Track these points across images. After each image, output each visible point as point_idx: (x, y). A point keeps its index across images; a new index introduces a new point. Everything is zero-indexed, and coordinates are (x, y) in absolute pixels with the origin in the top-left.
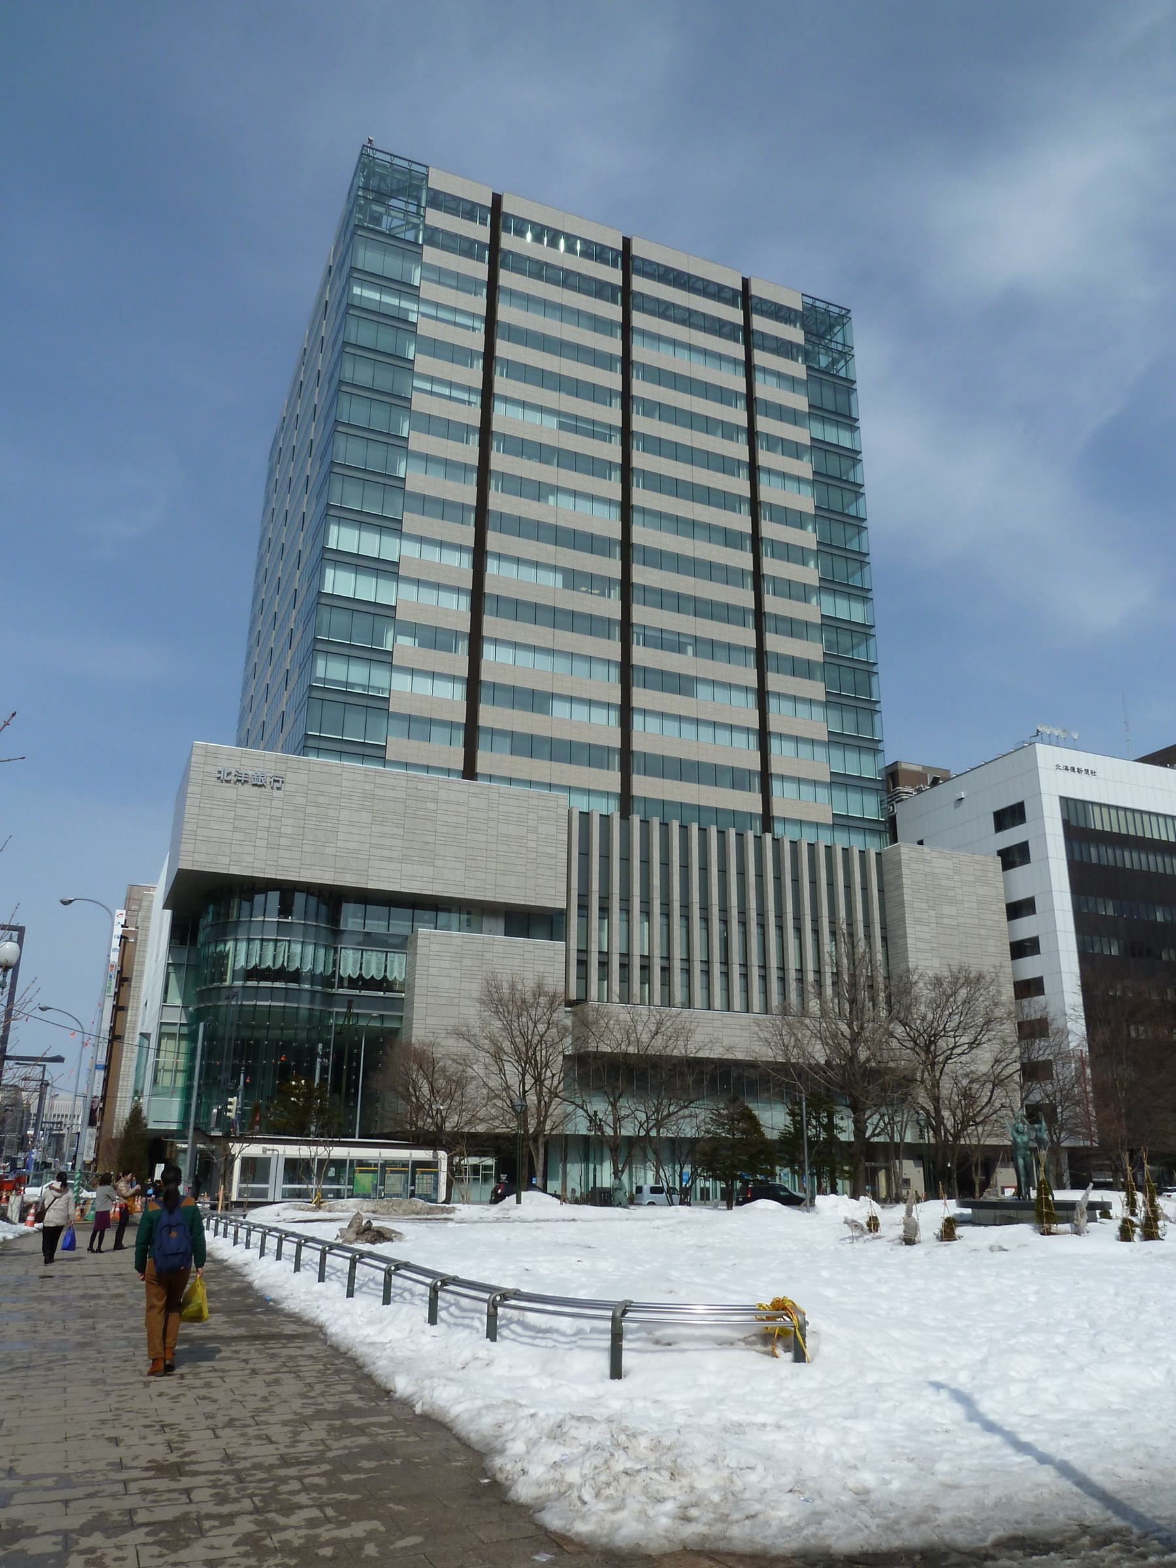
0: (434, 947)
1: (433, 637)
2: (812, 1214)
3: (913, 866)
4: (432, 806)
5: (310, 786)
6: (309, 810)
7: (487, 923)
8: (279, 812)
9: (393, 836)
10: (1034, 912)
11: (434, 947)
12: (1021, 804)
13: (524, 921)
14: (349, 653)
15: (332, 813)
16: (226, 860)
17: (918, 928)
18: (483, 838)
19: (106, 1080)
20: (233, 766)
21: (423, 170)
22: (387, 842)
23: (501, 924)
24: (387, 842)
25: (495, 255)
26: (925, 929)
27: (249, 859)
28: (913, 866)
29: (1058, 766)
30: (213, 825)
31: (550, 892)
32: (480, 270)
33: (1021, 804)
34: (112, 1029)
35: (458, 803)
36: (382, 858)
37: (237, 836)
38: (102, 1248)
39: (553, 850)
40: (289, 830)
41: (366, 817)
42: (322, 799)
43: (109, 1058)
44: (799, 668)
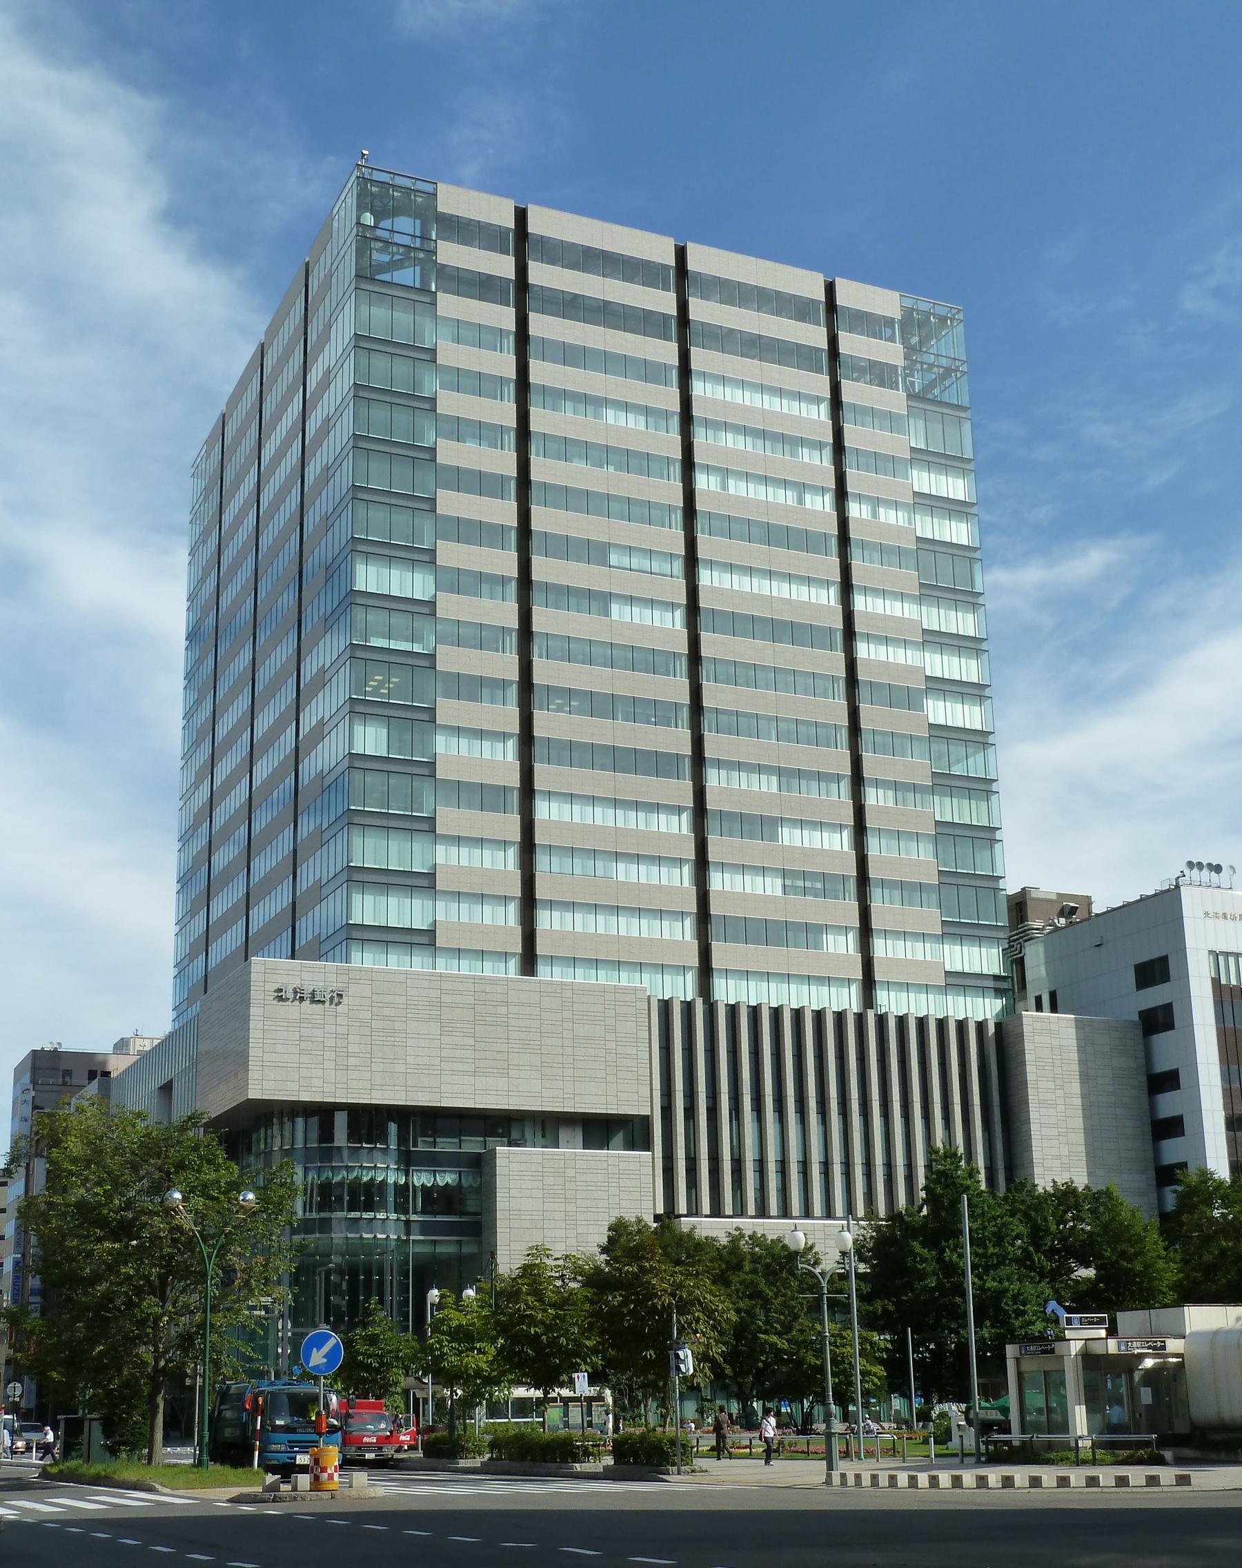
1: (483, 796)
3: (1037, 1039)
4: (503, 1010)
5: (375, 997)
7: (564, 1134)
8: (344, 1030)
10: (1179, 1088)
11: (514, 1166)
12: (1166, 957)
13: (600, 1129)
14: (387, 824)
15: (398, 1026)
16: (295, 1086)
17: (1043, 1111)
20: (290, 983)
21: (429, 188)
22: (457, 1053)
23: (579, 1136)
24: (457, 1053)
25: (522, 292)
26: (1052, 1112)
27: (318, 1082)
28: (1037, 1039)
29: (1207, 914)
30: (280, 1049)
31: (635, 1095)
32: (505, 317)
33: (1166, 957)
36: (454, 1072)
37: (305, 1059)
42: (387, 1012)
44: (908, 890)
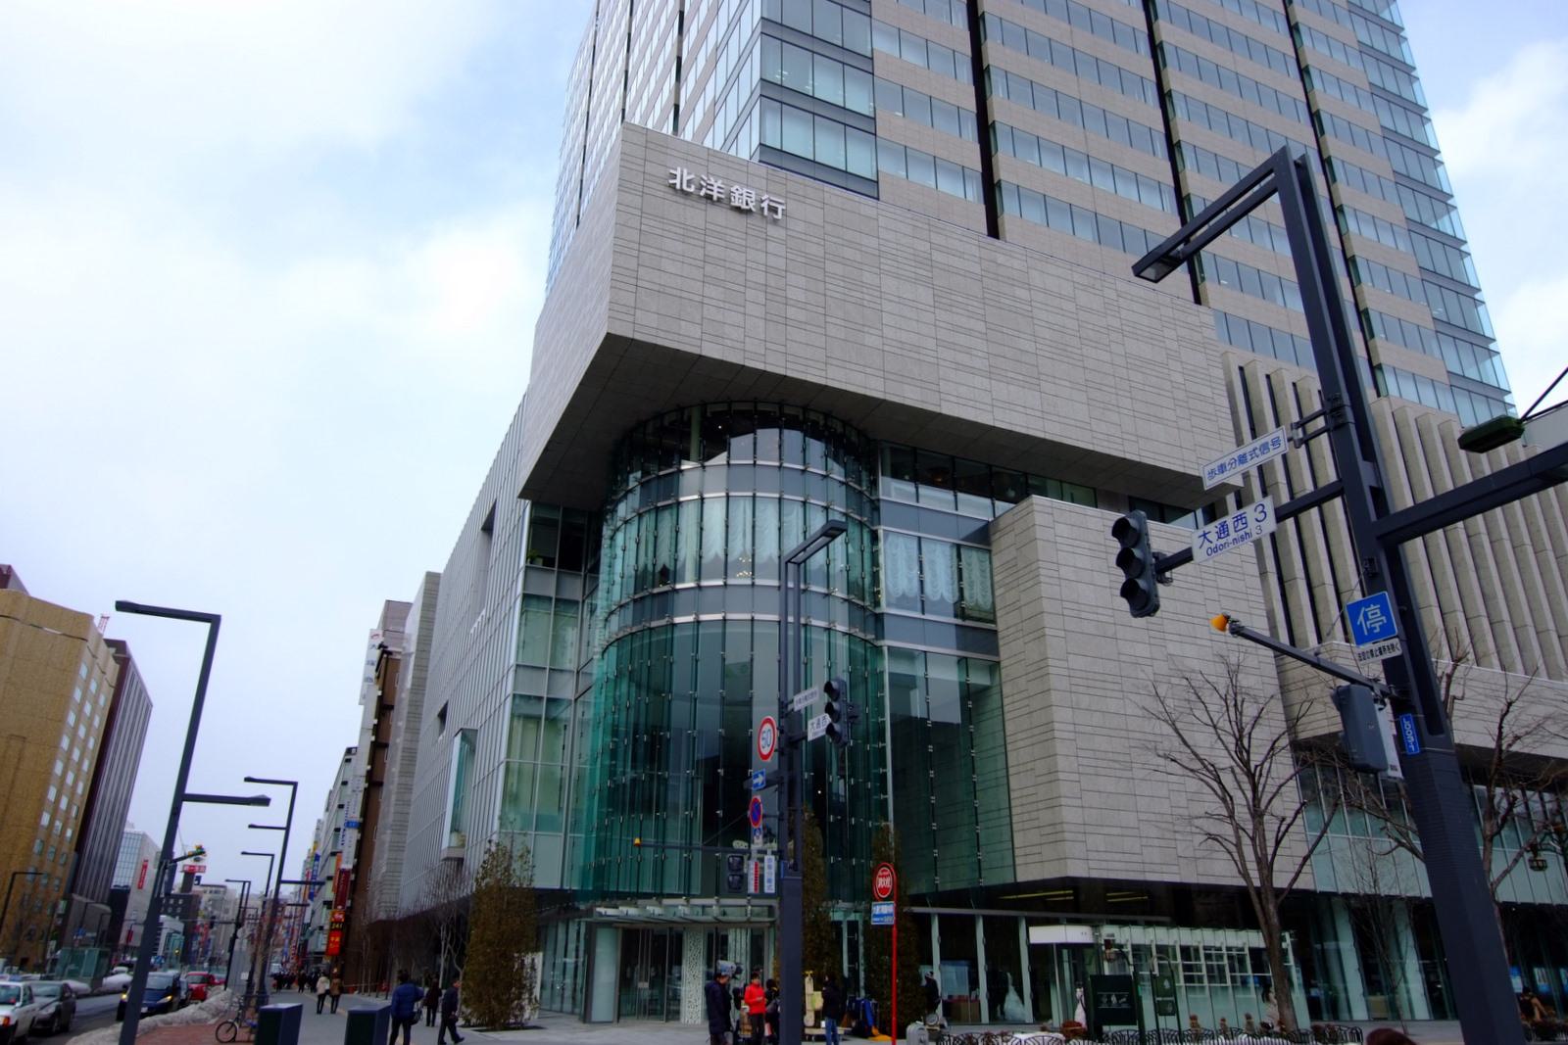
0: (1061, 529)
2: (672, 1024)
4: (1022, 293)
6: (830, 267)
9: (969, 332)
15: (867, 277)
18: (1106, 357)
19: (360, 844)
22: (961, 339)
24: (961, 339)
30: (667, 265)
34: (370, 775)
35: (1061, 297)
36: (958, 366)
38: (237, 1039)
39: (1207, 392)
40: (801, 296)
41: (925, 295)
42: (849, 253)
43: (365, 813)
